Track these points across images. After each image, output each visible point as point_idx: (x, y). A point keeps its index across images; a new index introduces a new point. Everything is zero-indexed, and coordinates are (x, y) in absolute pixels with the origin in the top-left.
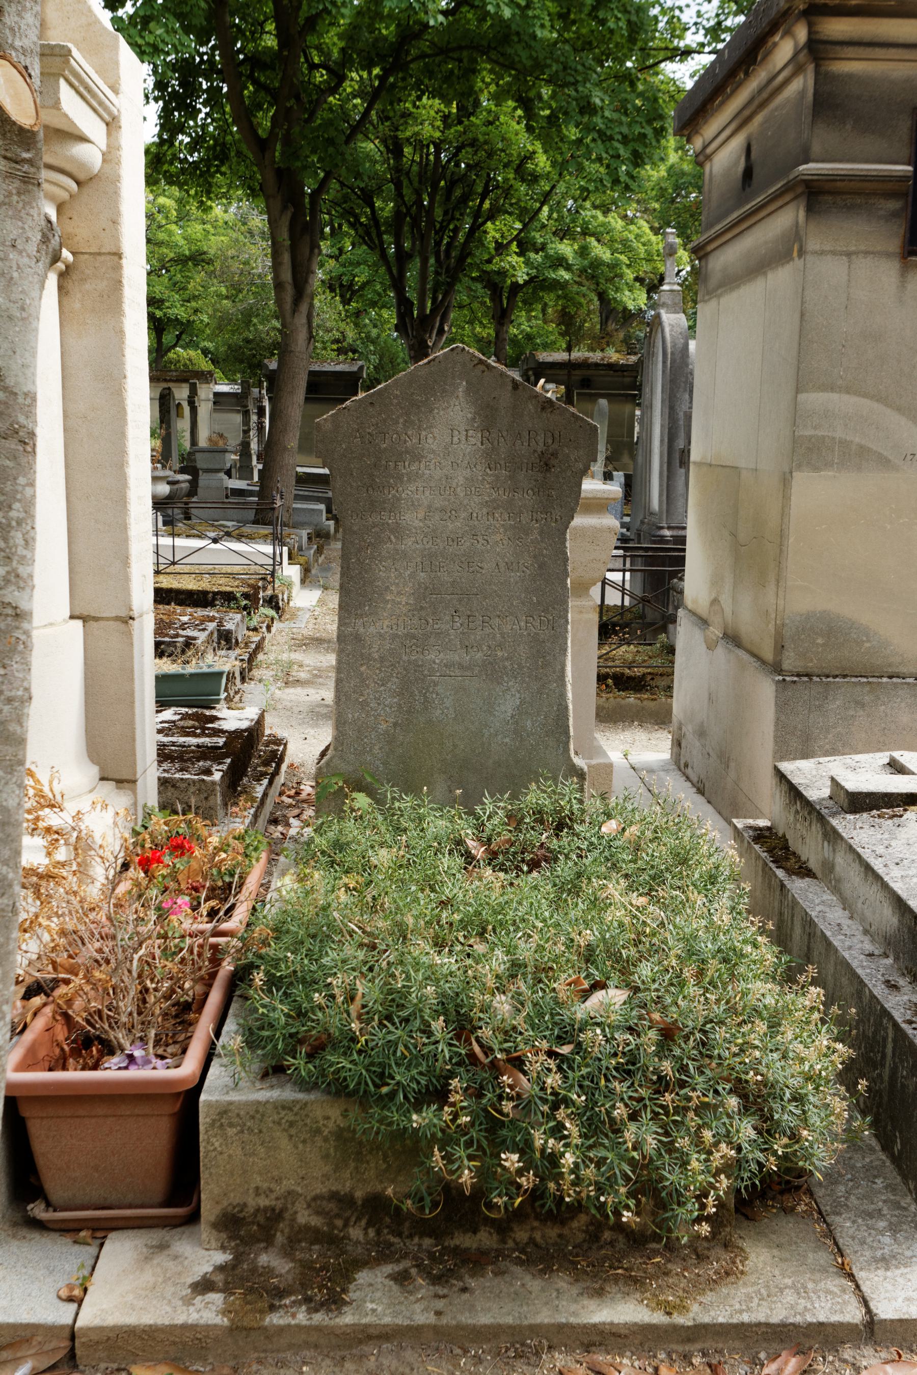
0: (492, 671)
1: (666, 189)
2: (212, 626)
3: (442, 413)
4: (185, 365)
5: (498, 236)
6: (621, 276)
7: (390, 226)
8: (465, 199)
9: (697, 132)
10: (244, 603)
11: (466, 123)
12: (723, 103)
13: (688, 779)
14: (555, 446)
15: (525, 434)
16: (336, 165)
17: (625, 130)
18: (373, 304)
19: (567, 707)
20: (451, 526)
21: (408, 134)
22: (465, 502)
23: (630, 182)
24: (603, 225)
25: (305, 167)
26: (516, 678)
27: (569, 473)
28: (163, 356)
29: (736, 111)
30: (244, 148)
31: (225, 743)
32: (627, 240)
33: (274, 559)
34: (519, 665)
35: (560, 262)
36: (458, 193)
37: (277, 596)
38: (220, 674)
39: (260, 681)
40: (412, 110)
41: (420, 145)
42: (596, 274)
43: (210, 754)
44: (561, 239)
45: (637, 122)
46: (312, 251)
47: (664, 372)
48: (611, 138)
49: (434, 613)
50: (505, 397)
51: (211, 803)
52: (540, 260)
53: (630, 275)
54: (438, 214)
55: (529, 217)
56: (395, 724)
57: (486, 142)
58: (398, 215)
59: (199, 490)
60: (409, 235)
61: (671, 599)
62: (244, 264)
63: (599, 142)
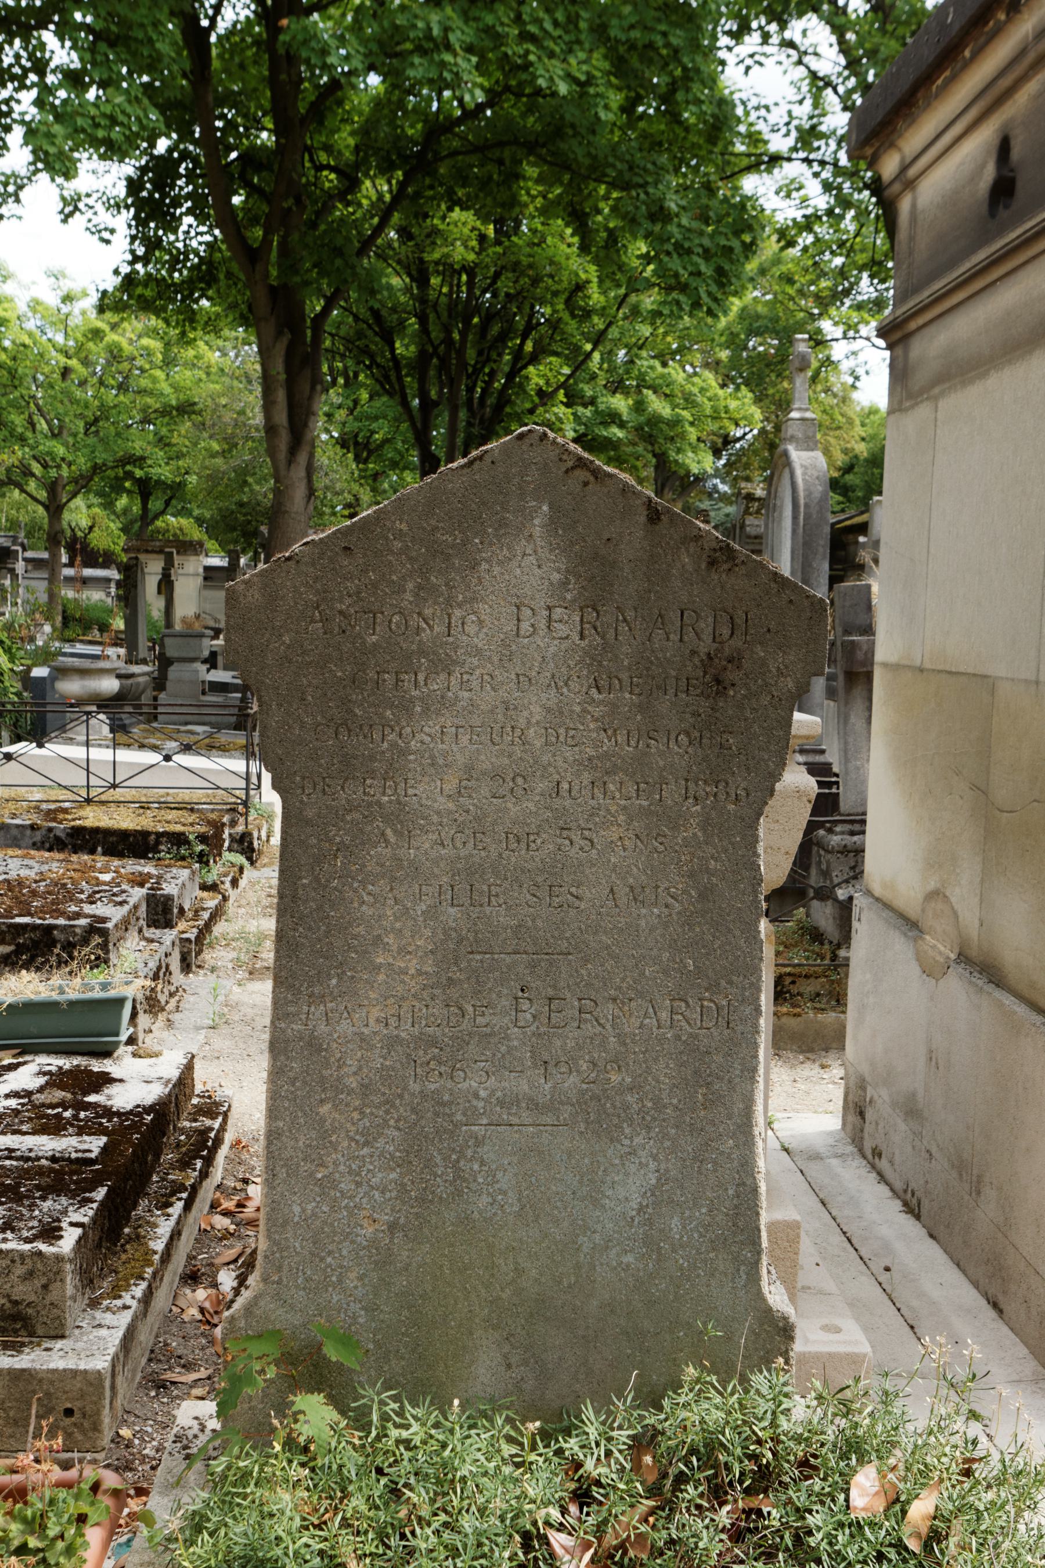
0: (599, 1115)
1: (738, 335)
2: (137, 894)
3: (497, 570)
4: (175, 535)
5: (542, 382)
6: (683, 436)
7: (413, 368)
8: (503, 338)
9: (892, 145)
10: (199, 848)
11: (507, 243)
12: (953, 78)
13: (882, 1178)
14: (737, 642)
15: (674, 616)
16: (345, 281)
17: (706, 242)
18: (394, 465)
19: (755, 1190)
20: (514, 810)
21: (436, 256)
22: (545, 759)
23: (714, 306)
24: (662, 376)
25: (307, 283)
26: (649, 1128)
27: (765, 700)
28: (148, 524)
29: (980, 86)
30: (235, 267)
31: (104, 1149)
32: (690, 394)
33: (248, 779)
34: (657, 1101)
35: (613, 418)
36: (495, 329)
37: (250, 834)
38: (120, 1002)
39: (213, 970)
40: (441, 227)
41: (449, 270)
42: (653, 433)
43: (64, 1177)
44: (614, 393)
45: (721, 233)
46: (313, 388)
47: (794, 531)
48: (689, 252)
49: (477, 993)
50: (633, 539)
51: (54, 1295)
52: (589, 414)
53: (692, 433)
54: (471, 355)
55: (579, 362)
56: (392, 1227)
57: (531, 266)
58: (423, 359)
59: (168, 684)
60: (435, 381)
61: (814, 859)
62: (239, 413)
63: (675, 256)
